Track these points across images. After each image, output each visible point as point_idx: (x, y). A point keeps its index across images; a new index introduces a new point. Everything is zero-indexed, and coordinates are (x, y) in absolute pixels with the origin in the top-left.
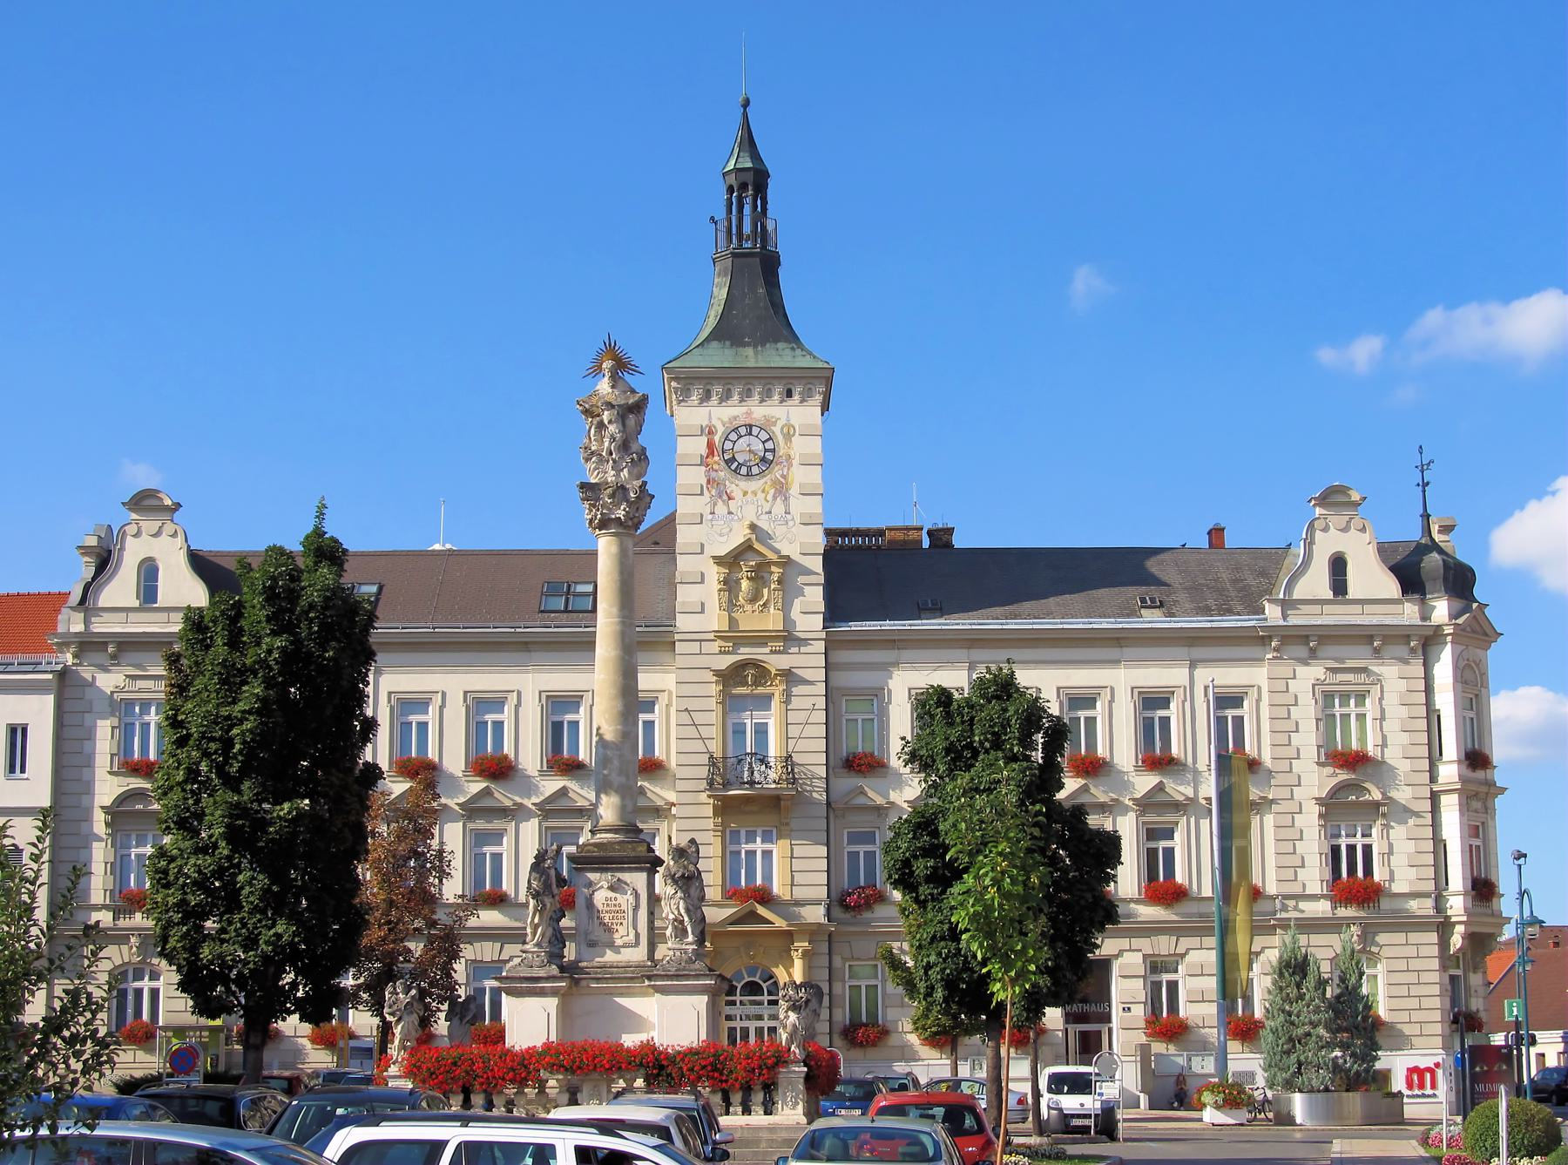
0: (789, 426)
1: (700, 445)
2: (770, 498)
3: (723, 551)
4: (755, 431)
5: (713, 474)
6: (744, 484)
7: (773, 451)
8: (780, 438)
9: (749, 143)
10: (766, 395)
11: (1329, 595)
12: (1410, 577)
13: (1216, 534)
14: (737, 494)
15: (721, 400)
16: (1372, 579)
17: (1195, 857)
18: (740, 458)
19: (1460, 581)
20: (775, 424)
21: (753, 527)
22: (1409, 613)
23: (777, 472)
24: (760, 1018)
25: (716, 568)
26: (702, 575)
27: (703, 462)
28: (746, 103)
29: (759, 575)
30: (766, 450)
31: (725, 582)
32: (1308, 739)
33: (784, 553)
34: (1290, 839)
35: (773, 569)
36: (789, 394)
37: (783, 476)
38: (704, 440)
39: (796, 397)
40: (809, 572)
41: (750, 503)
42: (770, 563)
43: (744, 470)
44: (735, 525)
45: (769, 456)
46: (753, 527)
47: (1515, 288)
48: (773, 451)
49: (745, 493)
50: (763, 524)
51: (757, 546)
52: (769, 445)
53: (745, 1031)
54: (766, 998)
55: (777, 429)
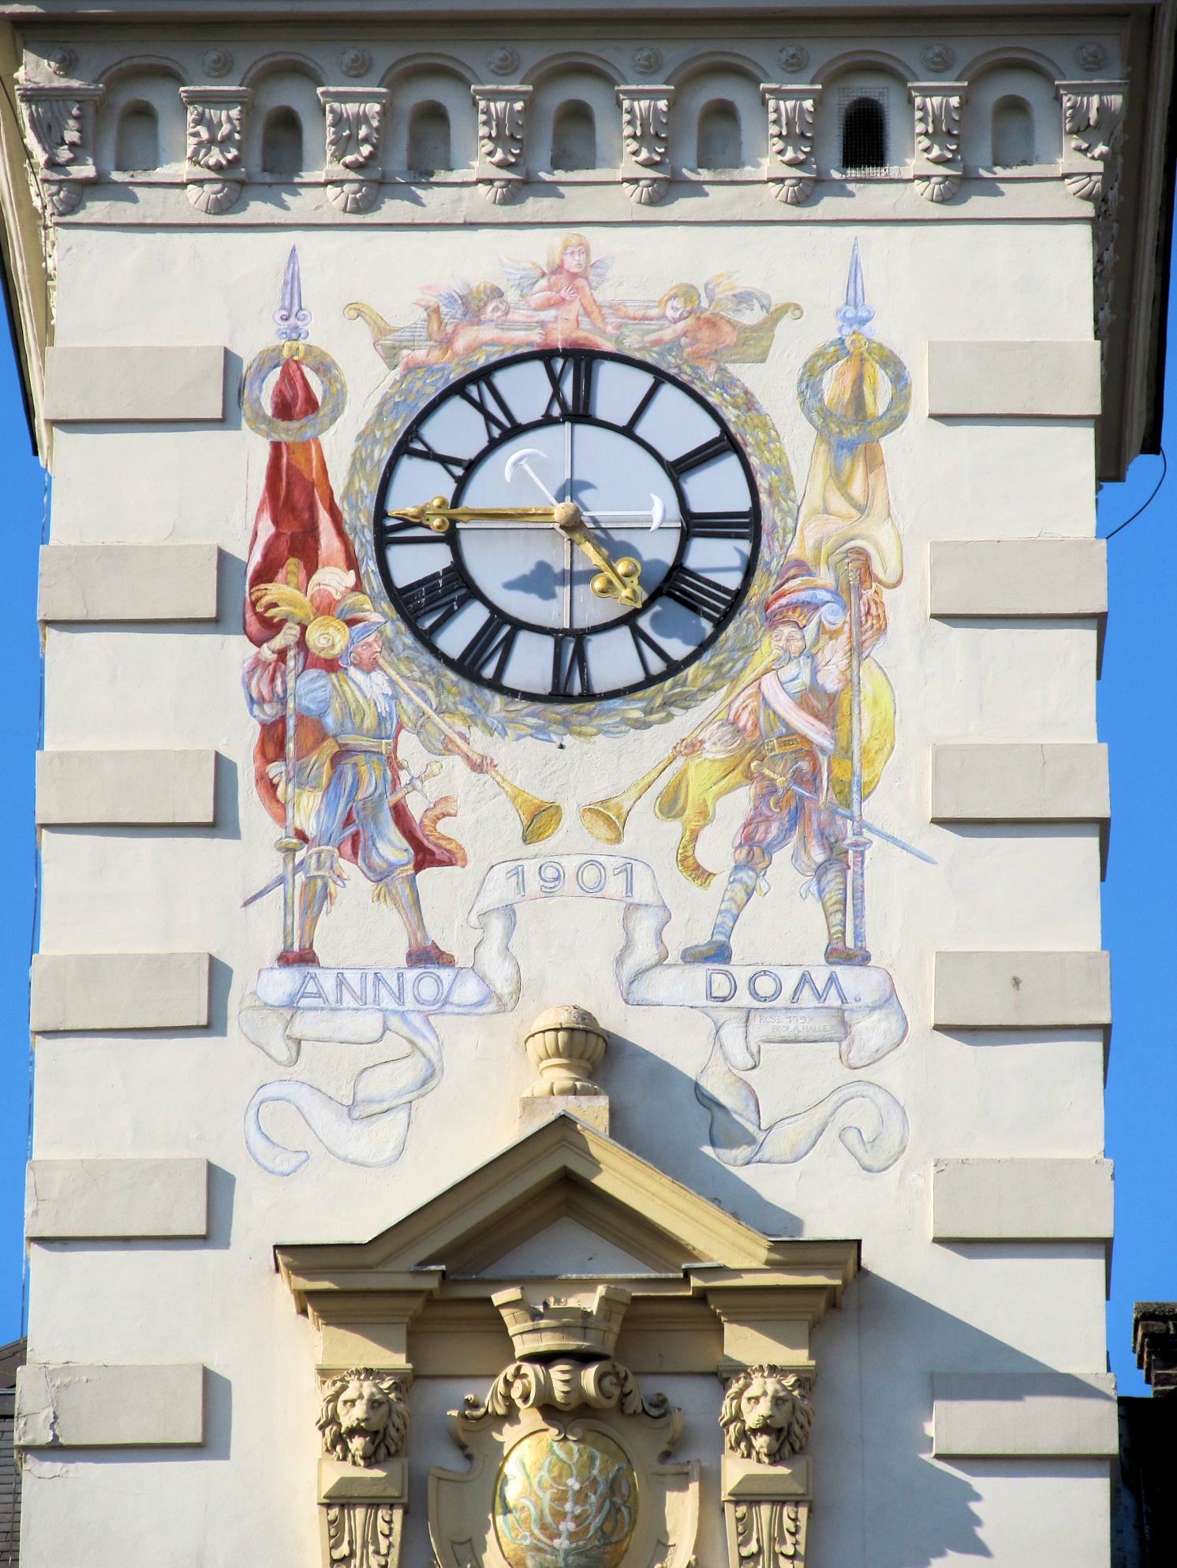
0: (859, 354)
1: (222, 491)
2: (718, 849)
3: (368, 1197)
4: (617, 391)
5: (307, 690)
6: (531, 757)
7: (747, 525)
8: (794, 443)
10: (694, 149)
15: (375, 184)
18: (494, 564)
20: (755, 343)
21: (592, 1051)
23: (769, 671)
25: (314, 1344)
26: (214, 1390)
27: (240, 603)
29: (634, 1390)
30: (695, 525)
31: (382, 1438)
33: (821, 1225)
35: (743, 1343)
36: (865, 142)
38: (246, 454)
39: (914, 157)
40: (1014, 1377)
41: (570, 895)
42: (712, 1303)
43: (531, 663)
44: (464, 1044)
45: (718, 559)
46: (592, 1051)
47: (79, 89)
48: (747, 525)
49: (539, 821)
50: (668, 1029)
51: (621, 1176)
52: (718, 489)
55: (772, 385)
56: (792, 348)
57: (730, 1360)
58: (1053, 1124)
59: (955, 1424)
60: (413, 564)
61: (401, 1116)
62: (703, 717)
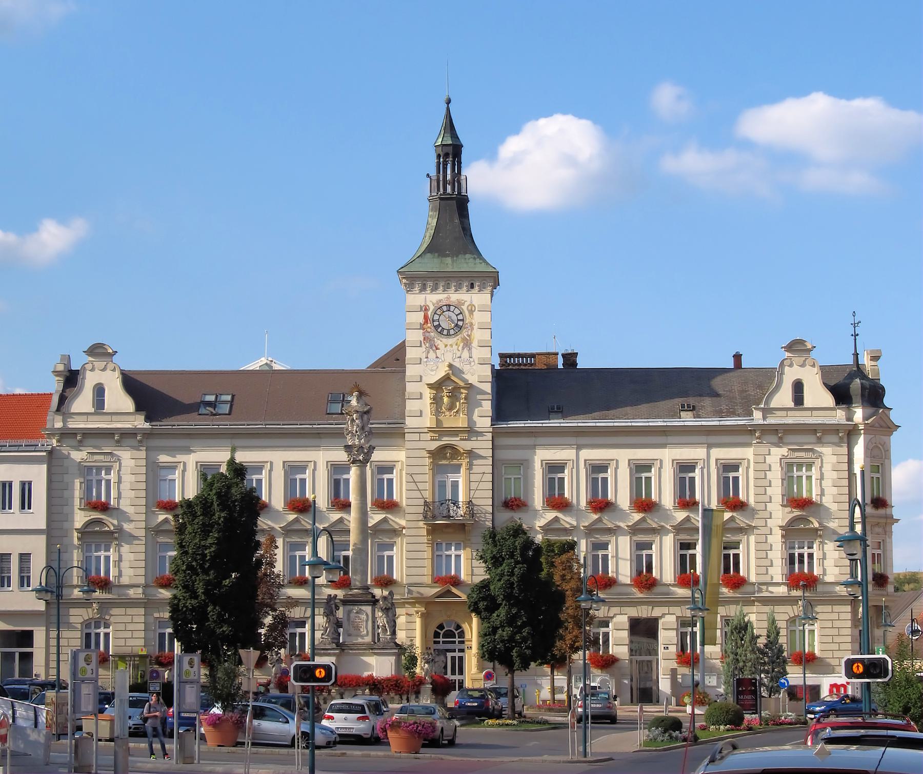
0: (472, 305)
1: (419, 317)
2: (460, 348)
3: (434, 378)
4: (452, 308)
5: (427, 334)
6: (445, 340)
7: (463, 320)
8: (467, 313)
9: (450, 127)
10: (458, 288)
11: (792, 405)
12: (841, 395)
13: (738, 357)
14: (441, 346)
15: (432, 291)
16: (818, 395)
17: (621, 563)
19: (874, 395)
20: (463, 304)
22: (839, 416)
23: (465, 333)
24: (454, 651)
25: (429, 390)
26: (421, 412)
27: (422, 327)
28: (449, 102)
32: (776, 491)
34: (764, 549)
35: (462, 391)
36: (472, 286)
37: (468, 336)
38: (422, 314)
39: (477, 288)
42: (460, 388)
43: (445, 332)
44: (440, 365)
45: (460, 323)
46: (451, 366)
48: (463, 320)
49: (446, 346)
50: (457, 364)
51: (453, 378)
52: (460, 317)
54: (457, 640)
55: (464, 308)
56: (466, 304)
59: (479, 397)
60: (436, 323)
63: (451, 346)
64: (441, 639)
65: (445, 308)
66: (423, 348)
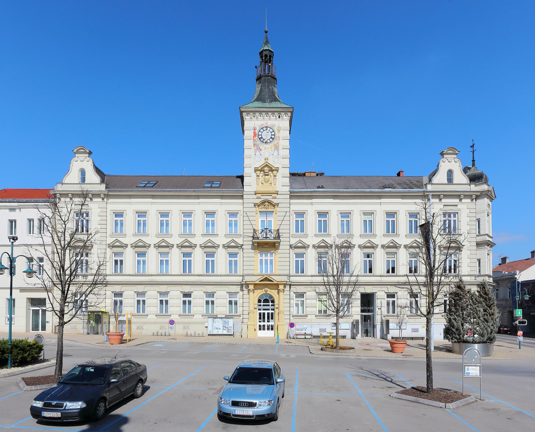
2: (273, 150)
5: (255, 142)
8: (276, 131)
11: (446, 182)
14: (262, 148)
18: (264, 137)
23: (275, 142)
24: (269, 310)
49: (265, 149)
52: (273, 133)
53: (264, 314)
55: (275, 129)
57: (261, 337)
58: (287, 162)
60: (260, 137)
61: (354, 274)
62: (272, 144)
63: (268, 148)
64: (262, 304)
65: (265, 129)
66: (253, 149)
